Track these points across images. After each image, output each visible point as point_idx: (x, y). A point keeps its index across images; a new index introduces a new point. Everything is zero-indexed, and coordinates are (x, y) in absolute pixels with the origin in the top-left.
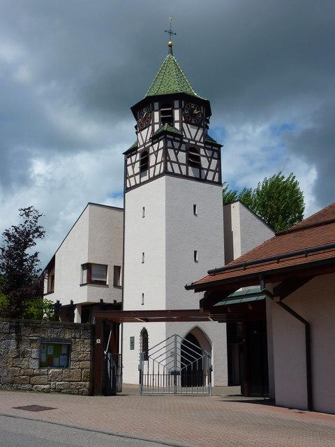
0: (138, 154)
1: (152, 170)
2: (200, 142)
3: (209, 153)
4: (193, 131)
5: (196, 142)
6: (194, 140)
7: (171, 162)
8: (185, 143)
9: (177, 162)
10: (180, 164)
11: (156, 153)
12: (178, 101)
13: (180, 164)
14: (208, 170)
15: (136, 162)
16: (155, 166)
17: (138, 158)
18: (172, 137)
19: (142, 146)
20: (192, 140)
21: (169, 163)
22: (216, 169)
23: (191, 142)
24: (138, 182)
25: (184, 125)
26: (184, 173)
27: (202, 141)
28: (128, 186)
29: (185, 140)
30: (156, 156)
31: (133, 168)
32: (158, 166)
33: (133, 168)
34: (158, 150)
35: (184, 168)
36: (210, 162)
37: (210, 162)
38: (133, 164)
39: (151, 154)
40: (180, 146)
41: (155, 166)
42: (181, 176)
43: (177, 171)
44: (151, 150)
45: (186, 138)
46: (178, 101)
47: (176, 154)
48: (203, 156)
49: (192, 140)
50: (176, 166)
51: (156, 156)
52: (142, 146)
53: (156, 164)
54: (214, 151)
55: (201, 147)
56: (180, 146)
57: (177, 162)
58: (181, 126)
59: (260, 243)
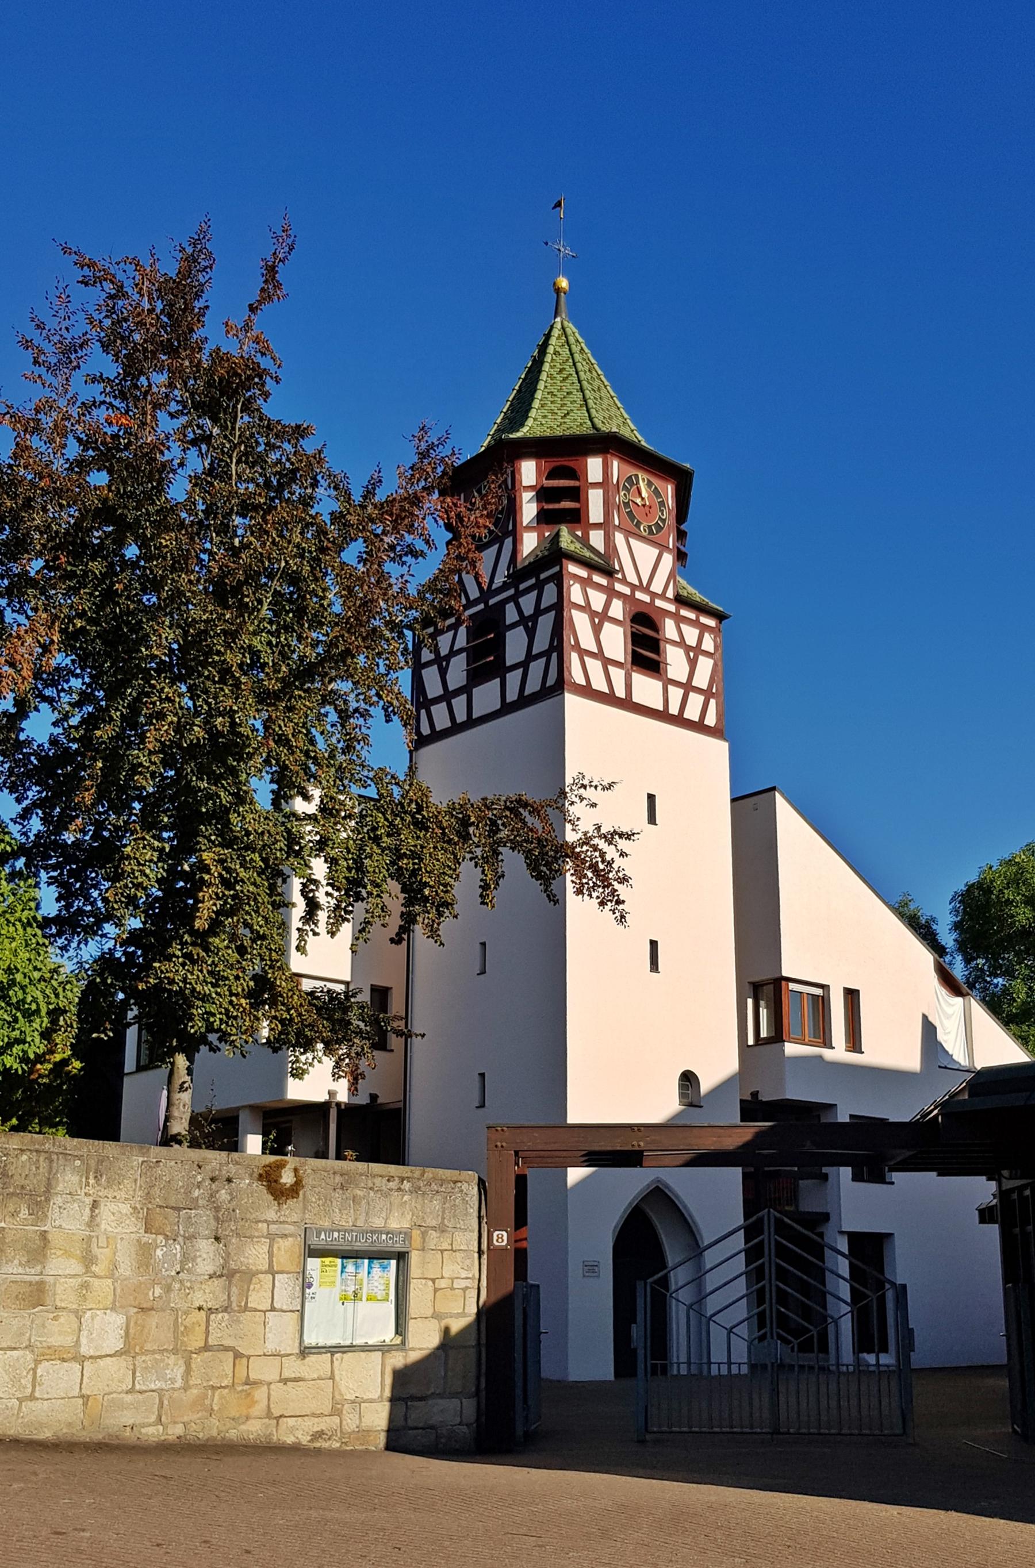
0: (462, 630)
1: (513, 679)
2: (663, 596)
4: (646, 553)
5: (654, 595)
6: (646, 590)
7: (583, 653)
8: (620, 595)
9: (599, 655)
10: (607, 662)
11: (529, 624)
12: (713, 1374)
13: (607, 662)
14: (688, 687)
15: (453, 653)
16: (524, 665)
17: (461, 641)
18: (583, 573)
19: (476, 602)
20: (641, 587)
21: (574, 657)
22: (710, 686)
23: (639, 595)
24: (461, 717)
25: (619, 538)
26: (620, 692)
27: (670, 594)
28: (425, 730)
29: (618, 587)
30: (531, 634)
31: (443, 673)
32: (536, 668)
33: (443, 673)
34: (538, 612)
35: (618, 675)
36: (693, 664)
37: (693, 664)
38: (442, 663)
39: (514, 625)
40: (607, 605)
41: (524, 665)
42: (608, 698)
43: (599, 684)
44: (511, 615)
45: (624, 581)
46: (713, 1374)
47: (597, 630)
48: (674, 643)
49: (641, 587)
50: (594, 666)
51: (531, 634)
52: (476, 602)
53: (530, 657)
54: (703, 628)
55: (667, 613)
56: (607, 605)
57: (599, 655)
58: (609, 540)
59: (954, 1514)
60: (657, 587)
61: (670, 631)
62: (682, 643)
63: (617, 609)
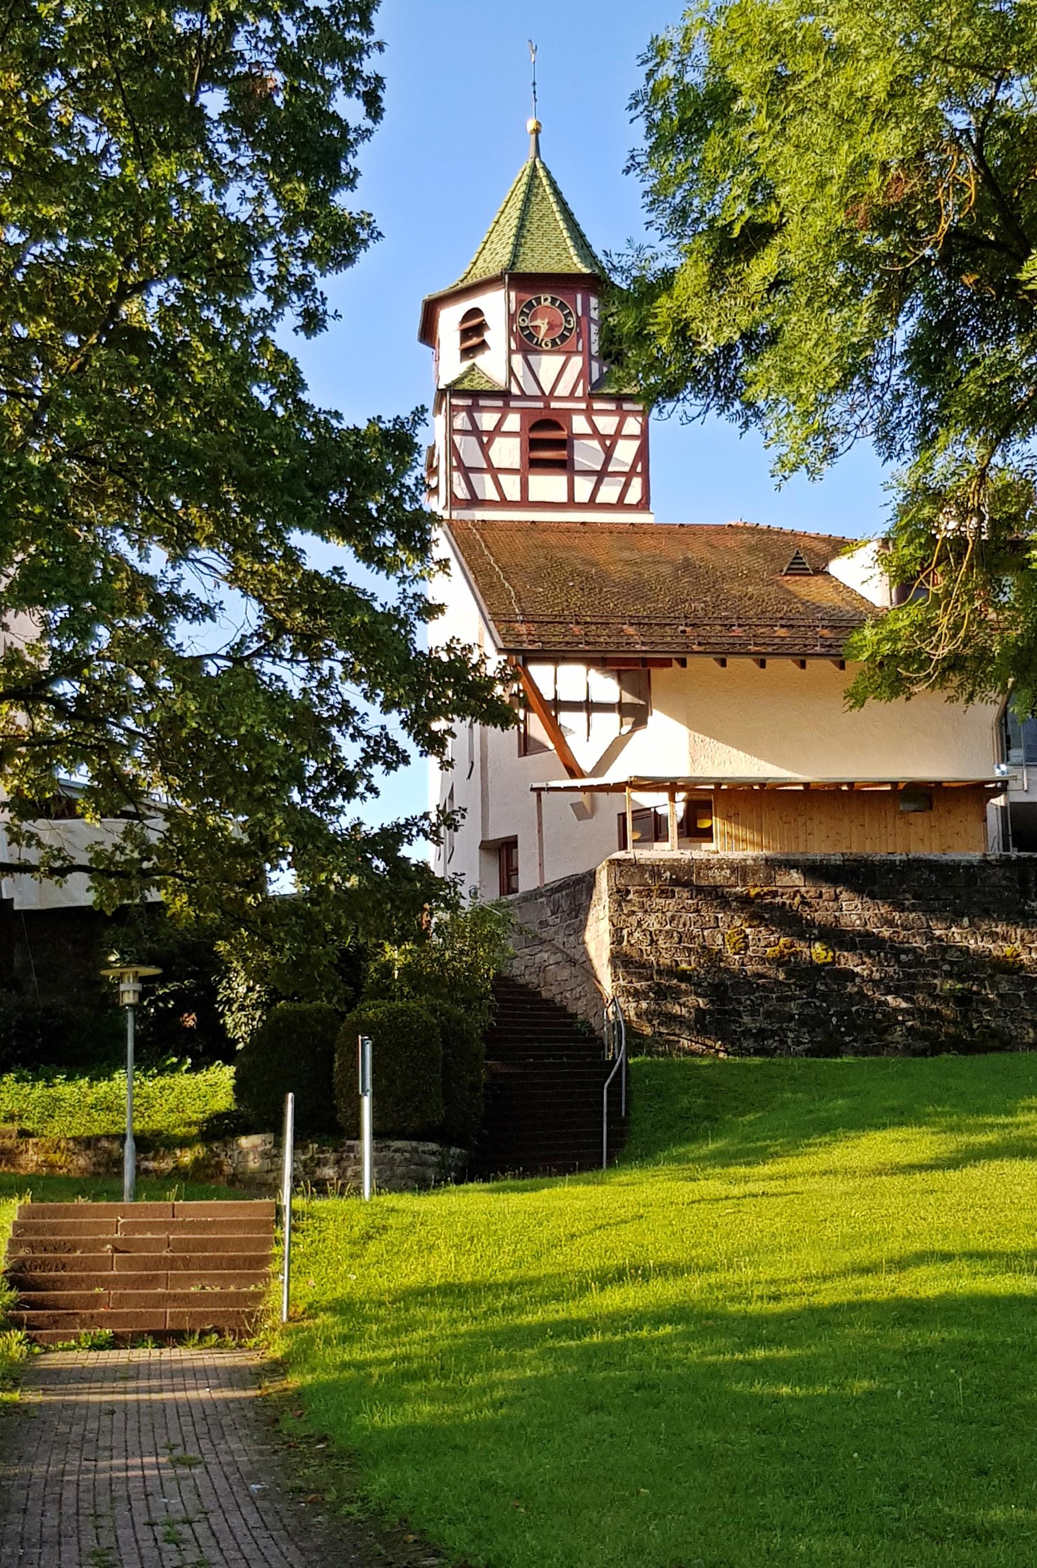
3: (607, 424)
13: (495, 472)
14: (601, 475)
22: (634, 466)
40: (620, 426)
60: (563, 390)
61: (580, 424)
62: (596, 434)
63: (513, 422)
